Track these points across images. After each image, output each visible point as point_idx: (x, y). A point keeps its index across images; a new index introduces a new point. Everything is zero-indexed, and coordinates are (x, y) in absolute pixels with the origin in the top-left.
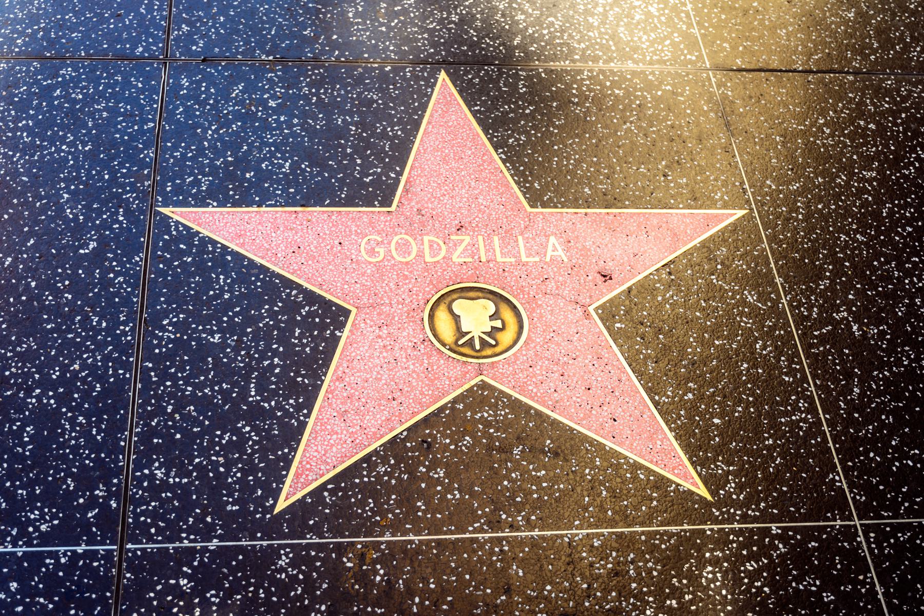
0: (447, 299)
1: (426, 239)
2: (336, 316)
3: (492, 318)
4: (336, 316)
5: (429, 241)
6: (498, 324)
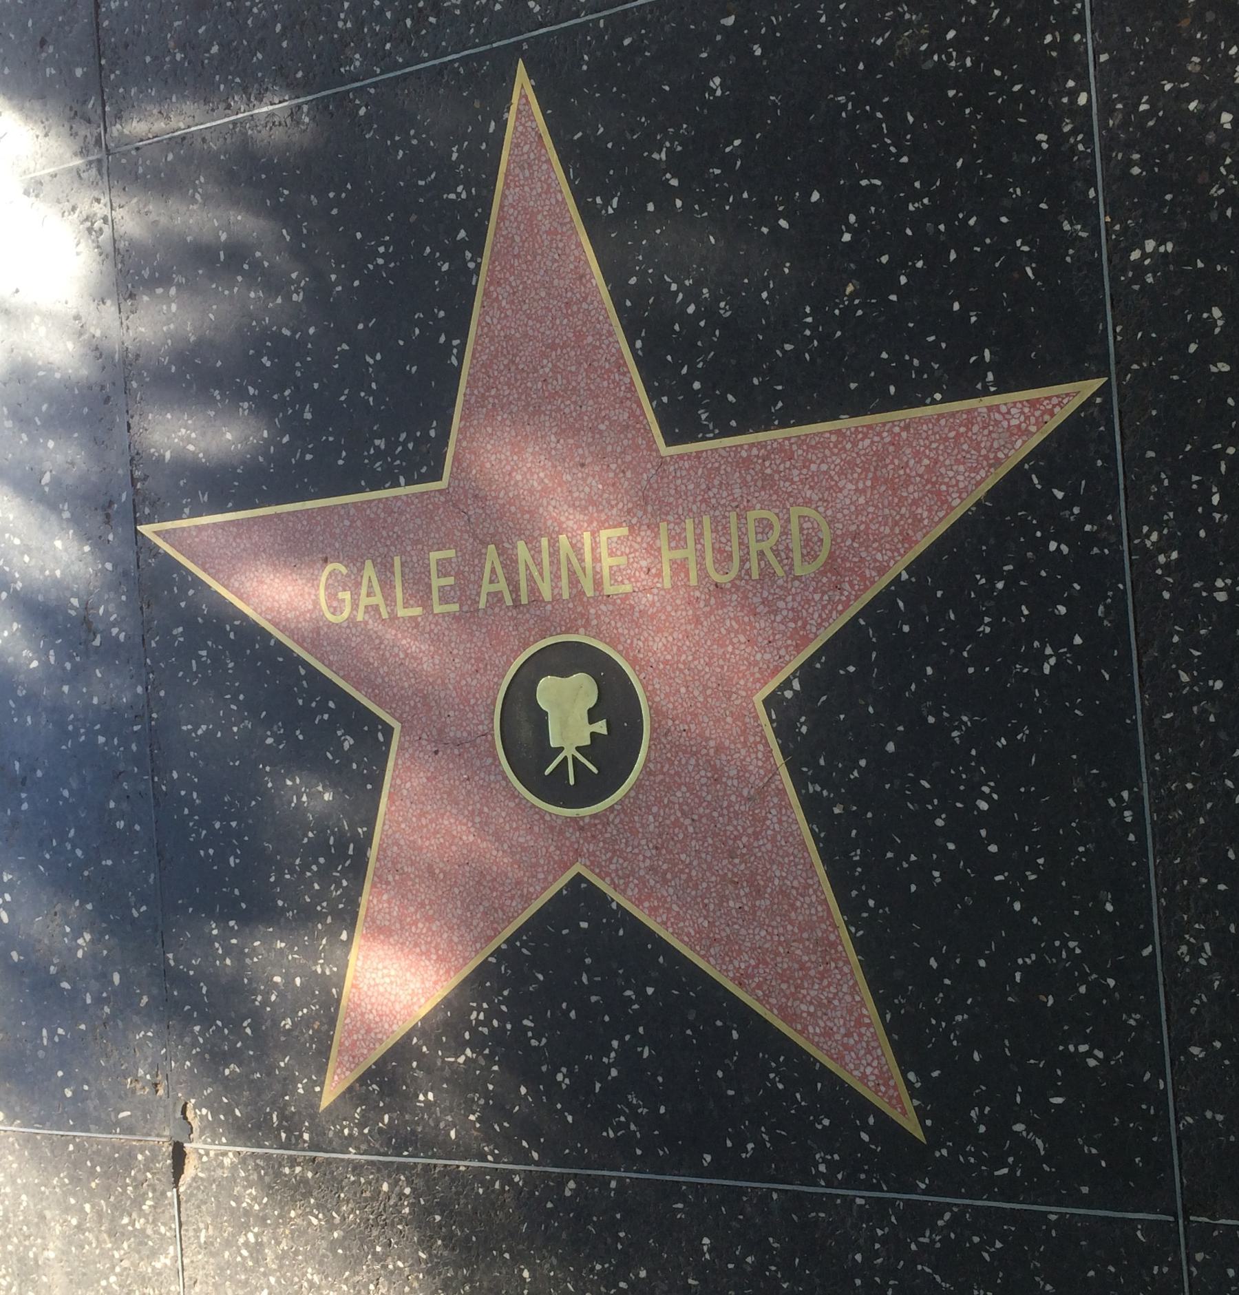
3: (593, 716)
6: (601, 727)
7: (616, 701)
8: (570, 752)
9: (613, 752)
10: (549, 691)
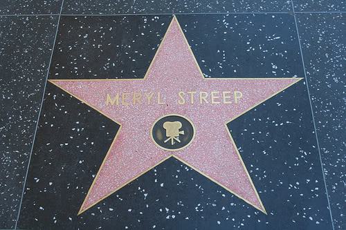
2: (113, 127)
3: (180, 130)
4: (113, 127)
6: (183, 133)
10: (166, 125)
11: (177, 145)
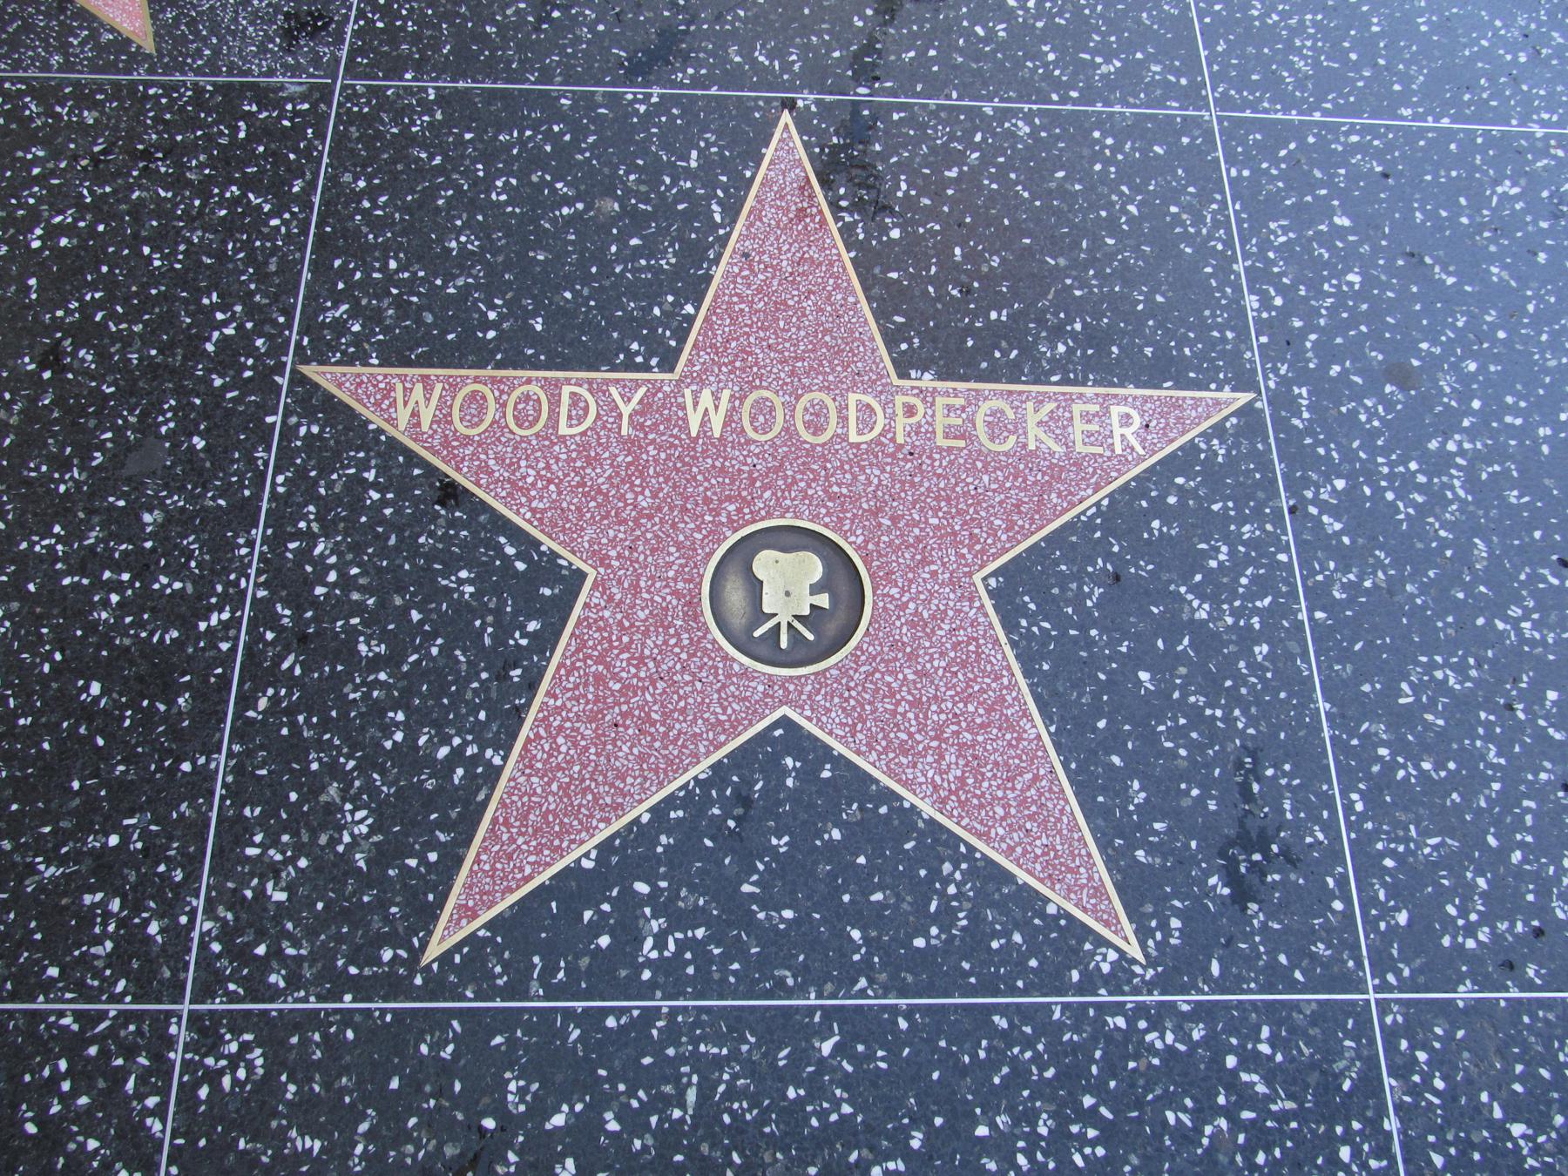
0: (744, 552)
1: (853, 398)
2: (544, 589)
3: (815, 589)
4: (544, 589)
5: (573, 394)
6: (823, 600)
7: (842, 576)
8: (784, 619)
9: (829, 630)
10: (766, 564)
11: (802, 654)
